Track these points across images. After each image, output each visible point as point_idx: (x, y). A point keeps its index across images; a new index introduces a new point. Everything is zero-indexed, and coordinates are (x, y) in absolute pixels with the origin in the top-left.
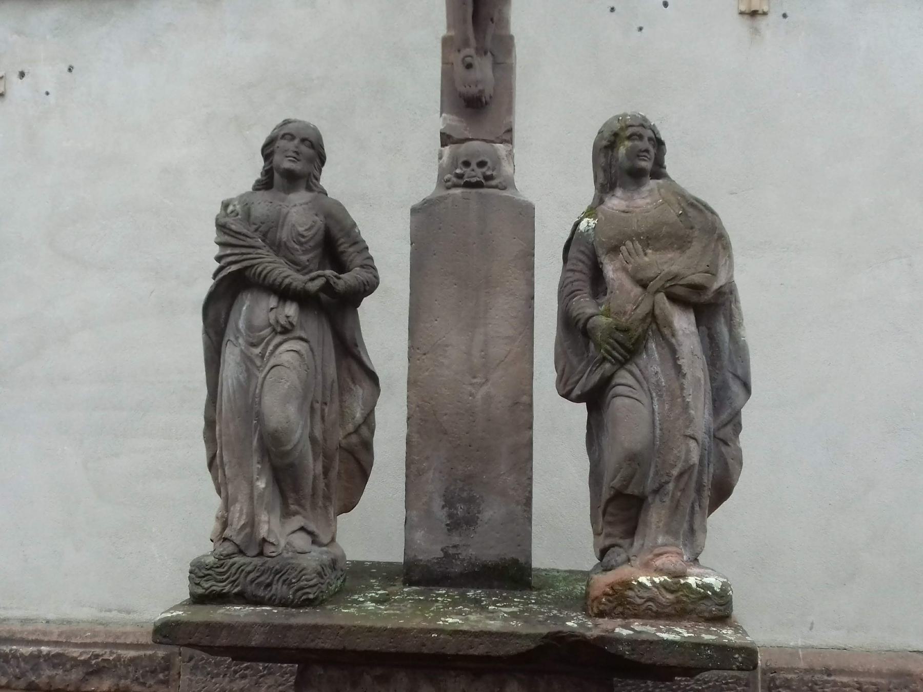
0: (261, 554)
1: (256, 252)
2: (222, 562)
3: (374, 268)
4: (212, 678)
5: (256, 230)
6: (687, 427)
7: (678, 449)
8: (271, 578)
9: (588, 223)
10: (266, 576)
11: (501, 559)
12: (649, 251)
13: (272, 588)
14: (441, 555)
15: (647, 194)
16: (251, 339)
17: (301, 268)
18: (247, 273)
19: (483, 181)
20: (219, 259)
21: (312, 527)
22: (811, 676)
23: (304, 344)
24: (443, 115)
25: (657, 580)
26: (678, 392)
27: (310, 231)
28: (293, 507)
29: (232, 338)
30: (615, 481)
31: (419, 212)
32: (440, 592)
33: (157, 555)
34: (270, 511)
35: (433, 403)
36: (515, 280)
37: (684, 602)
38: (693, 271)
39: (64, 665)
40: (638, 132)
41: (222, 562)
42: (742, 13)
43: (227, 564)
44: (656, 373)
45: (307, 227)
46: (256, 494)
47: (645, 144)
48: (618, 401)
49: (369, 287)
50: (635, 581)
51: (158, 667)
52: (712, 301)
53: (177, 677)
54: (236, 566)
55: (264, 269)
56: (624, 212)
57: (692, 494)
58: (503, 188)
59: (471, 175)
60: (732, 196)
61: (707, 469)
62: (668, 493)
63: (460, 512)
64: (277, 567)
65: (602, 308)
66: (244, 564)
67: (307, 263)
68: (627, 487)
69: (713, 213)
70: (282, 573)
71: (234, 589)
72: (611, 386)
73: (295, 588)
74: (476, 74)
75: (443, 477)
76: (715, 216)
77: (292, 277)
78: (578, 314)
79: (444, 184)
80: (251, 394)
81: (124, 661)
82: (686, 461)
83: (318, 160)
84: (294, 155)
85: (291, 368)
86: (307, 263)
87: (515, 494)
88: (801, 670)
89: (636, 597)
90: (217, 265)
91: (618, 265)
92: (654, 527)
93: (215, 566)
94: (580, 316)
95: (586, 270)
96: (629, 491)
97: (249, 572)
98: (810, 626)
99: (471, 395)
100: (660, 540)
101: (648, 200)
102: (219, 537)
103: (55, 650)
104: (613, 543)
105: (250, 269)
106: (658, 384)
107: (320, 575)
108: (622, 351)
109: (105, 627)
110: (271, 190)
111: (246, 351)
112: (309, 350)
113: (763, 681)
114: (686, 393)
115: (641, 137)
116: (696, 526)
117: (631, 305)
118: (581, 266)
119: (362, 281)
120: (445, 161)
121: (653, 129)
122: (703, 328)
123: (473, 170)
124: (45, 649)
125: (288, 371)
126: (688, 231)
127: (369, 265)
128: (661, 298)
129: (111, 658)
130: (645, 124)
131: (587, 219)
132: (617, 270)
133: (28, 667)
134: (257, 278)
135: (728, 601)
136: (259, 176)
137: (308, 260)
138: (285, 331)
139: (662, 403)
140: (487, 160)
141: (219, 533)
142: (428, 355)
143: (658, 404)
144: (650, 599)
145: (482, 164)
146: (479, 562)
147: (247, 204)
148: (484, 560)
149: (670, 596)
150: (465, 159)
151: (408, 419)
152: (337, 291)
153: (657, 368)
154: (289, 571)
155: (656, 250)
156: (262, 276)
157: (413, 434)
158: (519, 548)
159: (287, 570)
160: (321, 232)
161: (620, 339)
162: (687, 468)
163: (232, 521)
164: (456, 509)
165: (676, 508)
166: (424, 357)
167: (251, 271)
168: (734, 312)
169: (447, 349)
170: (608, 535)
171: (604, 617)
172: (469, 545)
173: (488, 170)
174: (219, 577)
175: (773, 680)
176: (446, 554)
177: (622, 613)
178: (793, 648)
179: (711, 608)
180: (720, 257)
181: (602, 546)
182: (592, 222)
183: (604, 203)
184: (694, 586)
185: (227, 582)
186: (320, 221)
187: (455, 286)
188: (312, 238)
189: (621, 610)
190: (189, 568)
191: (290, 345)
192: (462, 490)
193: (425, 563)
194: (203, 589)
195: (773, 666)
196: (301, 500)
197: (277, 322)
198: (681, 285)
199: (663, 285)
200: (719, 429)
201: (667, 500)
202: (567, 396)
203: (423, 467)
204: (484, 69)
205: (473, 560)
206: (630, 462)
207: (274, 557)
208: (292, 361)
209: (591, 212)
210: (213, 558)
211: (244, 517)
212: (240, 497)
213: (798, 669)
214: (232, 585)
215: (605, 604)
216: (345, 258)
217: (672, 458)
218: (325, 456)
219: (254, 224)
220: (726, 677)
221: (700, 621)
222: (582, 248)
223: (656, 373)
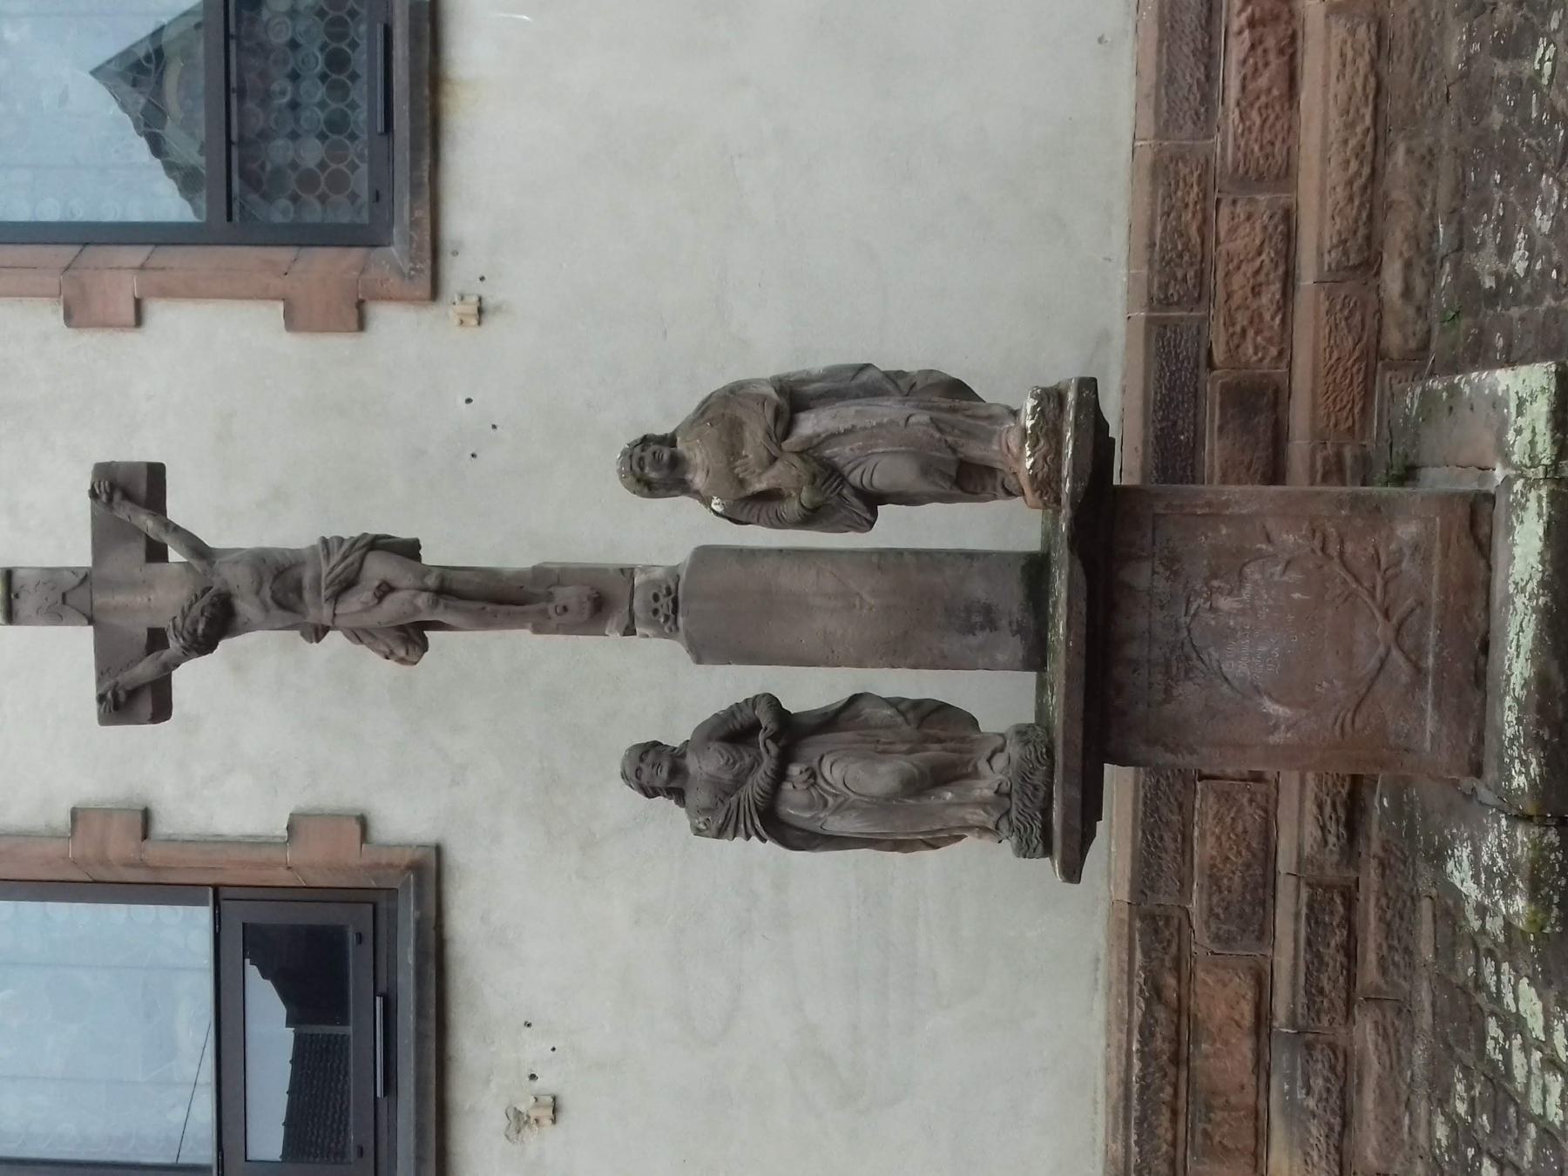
3: (756, 696)
4: (1162, 871)
5: (722, 802)
6: (898, 425)
12: (744, 453)
14: (1018, 636)
17: (757, 762)
18: (762, 809)
20: (748, 837)
21: (988, 753)
23: (824, 760)
25: (1028, 453)
28: (970, 769)
29: (820, 823)
37: (1047, 430)
39: (1150, 1025)
42: (479, 323)
44: (852, 449)
46: (956, 801)
47: (648, 455)
48: (876, 482)
49: (773, 702)
53: (1162, 908)
54: (1019, 817)
56: (708, 474)
57: (959, 417)
64: (1019, 780)
65: (794, 494)
68: (950, 476)
69: (710, 396)
74: (573, 604)
79: (673, 632)
80: (869, 806)
90: (754, 839)
91: (756, 480)
92: (985, 453)
95: (758, 506)
97: (1025, 805)
99: (871, 609)
101: (698, 453)
103: (1136, 1036)
106: (860, 448)
107: (1027, 743)
108: (832, 480)
113: (1161, 311)
114: (869, 426)
115: (641, 459)
118: (755, 511)
121: (633, 446)
122: (812, 403)
124: (1135, 1047)
127: (753, 702)
128: (786, 445)
133: (1154, 1063)
138: (813, 775)
139: (877, 446)
145: (656, 598)
149: (1042, 442)
150: (651, 614)
151: (893, 667)
155: (743, 447)
156: (761, 793)
164: (976, 623)
165: (969, 434)
170: (994, 489)
176: (1018, 632)
177: (1057, 483)
178: (1129, 279)
181: (1003, 495)
182: (716, 500)
184: (1033, 422)
186: (715, 745)
190: (1022, 859)
195: (1145, 300)
197: (805, 782)
200: (900, 391)
201: (961, 441)
202: (871, 524)
204: (564, 594)
209: (706, 502)
211: (977, 811)
213: (1148, 276)
218: (925, 742)
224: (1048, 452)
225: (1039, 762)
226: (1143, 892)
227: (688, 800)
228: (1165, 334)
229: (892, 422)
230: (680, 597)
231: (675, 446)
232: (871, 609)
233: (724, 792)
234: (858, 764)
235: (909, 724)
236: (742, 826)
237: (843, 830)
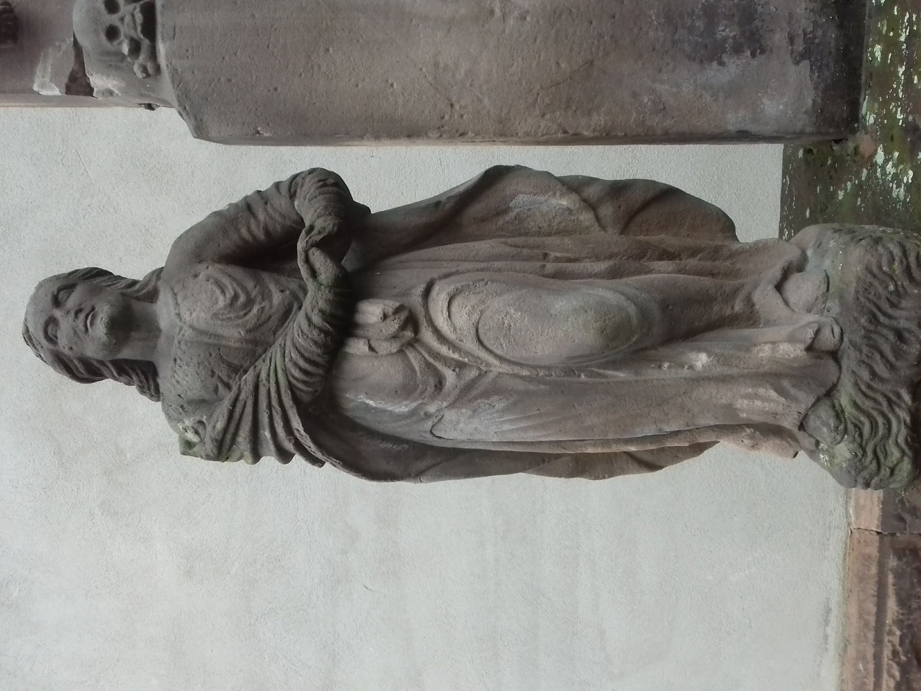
0: (834, 355)
1: (264, 382)
2: (850, 427)
3: (295, 177)
5: (228, 386)
8: (885, 331)
10: (880, 341)
13: (905, 329)
14: (805, 64)
16: (429, 388)
18: (306, 398)
20: (285, 456)
21: (775, 272)
27: (226, 287)
29: (429, 424)
31: (201, 120)
33: (747, 572)
34: (748, 346)
41: (850, 427)
43: (856, 419)
45: (218, 292)
46: (718, 370)
51: (914, 566)
54: (860, 400)
55: (296, 364)
59: (131, 23)
63: (730, 31)
66: (856, 384)
67: (288, 292)
70: (875, 310)
71: (904, 402)
73: (906, 283)
77: (309, 311)
81: (903, 614)
83: (98, 280)
84: (82, 316)
85: (482, 307)
86: (288, 292)
93: (858, 439)
97: (874, 374)
102: (792, 443)
105: (298, 393)
109: (850, 644)
110: (155, 362)
111: (451, 399)
112: (447, 280)
119: (317, 188)
120: (115, 83)
123: (122, 19)
125: (488, 313)
129: (898, 633)
134: (314, 380)
136: (133, 390)
137: (282, 291)
138: (411, 322)
141: (784, 442)
142: (454, 99)
147: (182, 407)
152: (336, 229)
154: (871, 297)
157: (593, 124)
159: (870, 301)
160: (231, 269)
162: (612, 292)
163: (767, 413)
164: (725, 39)
166: (457, 107)
167: (301, 390)
169: (442, 65)
172: (790, 14)
174: (881, 431)
185: (890, 416)
188: (239, 284)
191: (439, 314)
193: (820, 94)
194: (902, 458)
196: (725, 292)
197: (395, 337)
203: (650, 103)
207: (842, 330)
208: (469, 307)
210: (842, 445)
211: (762, 391)
212: (723, 401)
214: (899, 407)
216: (277, 228)
219: (216, 390)
225: (911, 279)
226: (901, 519)
227: (164, 383)
232: (523, 18)
233: (230, 365)
234: (507, 297)
235: (603, 228)
236: (267, 434)
237: (477, 437)
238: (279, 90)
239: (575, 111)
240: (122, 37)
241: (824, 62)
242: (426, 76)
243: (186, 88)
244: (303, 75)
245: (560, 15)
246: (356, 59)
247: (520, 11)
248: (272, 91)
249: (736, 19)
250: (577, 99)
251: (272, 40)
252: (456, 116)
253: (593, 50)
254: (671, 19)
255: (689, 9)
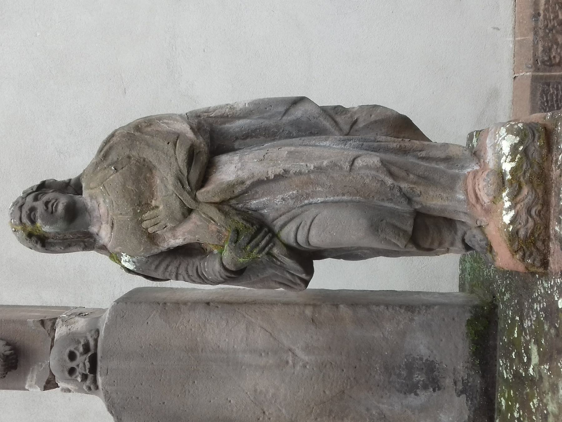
6: (341, 168)
7: (365, 178)
9: (126, 261)
11: (467, 336)
14: (463, 397)
15: (94, 201)
19: (90, 354)
22: (540, 30)
24: (26, 388)
26: (304, 178)
30: (398, 244)
31: (121, 419)
32: (503, 404)
35: (312, 404)
36: (190, 322)
37: (531, 175)
38: (173, 160)
40: (26, 212)
44: (283, 199)
47: (40, 206)
50: (510, 227)
52: (208, 135)
56: (112, 227)
57: (410, 159)
58: (97, 333)
60: (127, 92)
61: (383, 143)
62: (412, 189)
65: (216, 251)
68: (405, 232)
69: (113, 135)
72: (297, 247)
75: (387, 394)
76: (116, 133)
78: (221, 277)
79: (94, 387)
82: (377, 169)
87: (403, 323)
88: (535, 38)
89: (526, 227)
91: (169, 235)
92: (446, 203)
94: (223, 275)
95: (176, 263)
96: (410, 229)
98: (496, 30)
99: (305, 366)
100: (461, 197)
101: (101, 200)
104: (461, 241)
106: (296, 198)
113: (545, 70)
114: (306, 171)
115: (33, 210)
116: (441, 154)
117: (210, 225)
118: (172, 268)
120: (72, 387)
122: (236, 145)
123: (78, 366)
126: (133, 161)
128: (202, 194)
130: (19, 205)
131: (122, 262)
132: (174, 236)
135: (530, 128)
139: (314, 194)
140: (67, 351)
142: (265, 409)
143: (317, 198)
144: (529, 211)
145: (72, 356)
146: (470, 360)
148: (468, 354)
149: (525, 190)
150: (66, 374)
153: (277, 199)
155: (152, 195)
158: (456, 319)
161: (247, 239)
162: (385, 169)
164: (418, 382)
166: (267, 413)
168: (219, 114)
169: (259, 390)
171: (549, 260)
172: (454, 369)
173: (78, 351)
175: (543, 62)
176: (462, 392)
177: (544, 242)
179: (537, 147)
180: (159, 129)
182: (125, 258)
183: (105, 245)
184: (513, 164)
187: (196, 382)
189: (541, 243)
192: (399, 376)
193: (472, 413)
195: (531, 62)
198: (188, 172)
199: (189, 193)
200: (341, 130)
201: (419, 189)
205: (469, 365)
206: (380, 230)
209: (116, 258)
215: (534, 260)
217: (375, 184)
220: (542, 102)
221: (551, 159)
222: (153, 267)
223: (283, 199)
224: (534, 202)
228: (548, 90)
229: (334, 165)
230: (99, 355)
231: (81, 193)
232: (305, 366)
238: (165, 404)
239: (334, 417)
240: (77, 373)
241: (474, 396)
242: (249, 397)
243: (112, 402)
244: (180, 395)
245: (326, 366)
246: (210, 387)
247: (303, 363)
248: (162, 404)
249: (424, 371)
250: (335, 411)
251: (162, 376)
252: (266, 419)
253: (344, 385)
254: (388, 369)
255: (397, 365)
